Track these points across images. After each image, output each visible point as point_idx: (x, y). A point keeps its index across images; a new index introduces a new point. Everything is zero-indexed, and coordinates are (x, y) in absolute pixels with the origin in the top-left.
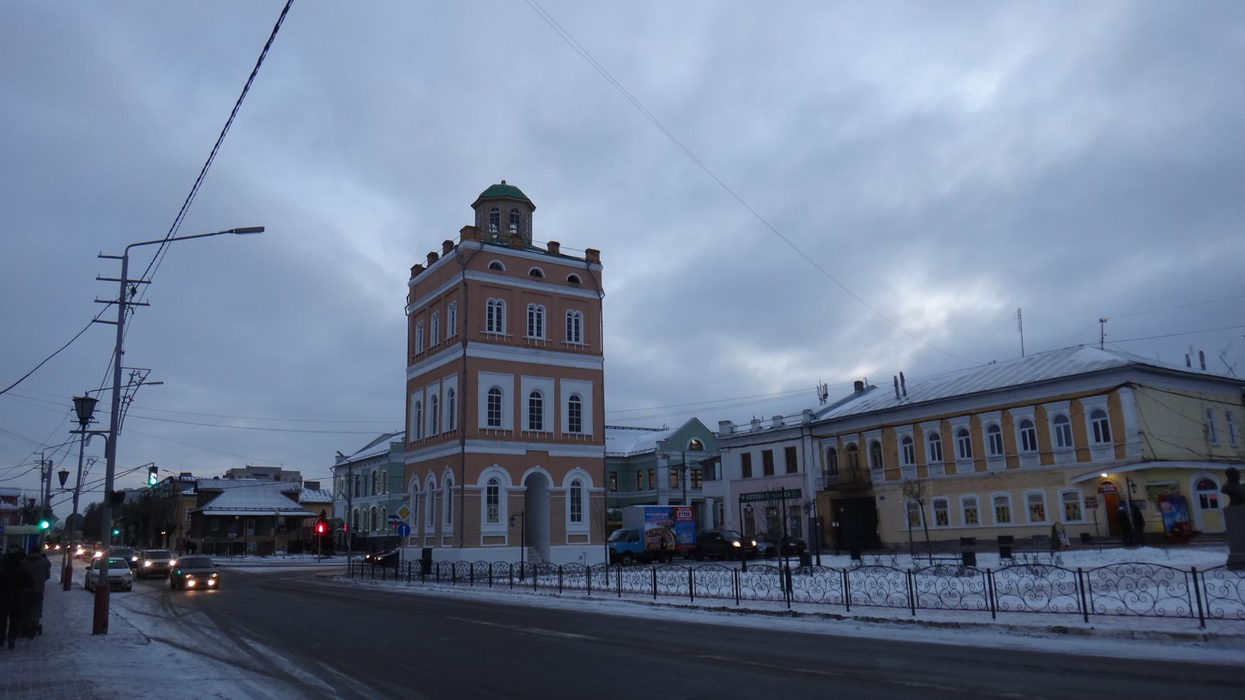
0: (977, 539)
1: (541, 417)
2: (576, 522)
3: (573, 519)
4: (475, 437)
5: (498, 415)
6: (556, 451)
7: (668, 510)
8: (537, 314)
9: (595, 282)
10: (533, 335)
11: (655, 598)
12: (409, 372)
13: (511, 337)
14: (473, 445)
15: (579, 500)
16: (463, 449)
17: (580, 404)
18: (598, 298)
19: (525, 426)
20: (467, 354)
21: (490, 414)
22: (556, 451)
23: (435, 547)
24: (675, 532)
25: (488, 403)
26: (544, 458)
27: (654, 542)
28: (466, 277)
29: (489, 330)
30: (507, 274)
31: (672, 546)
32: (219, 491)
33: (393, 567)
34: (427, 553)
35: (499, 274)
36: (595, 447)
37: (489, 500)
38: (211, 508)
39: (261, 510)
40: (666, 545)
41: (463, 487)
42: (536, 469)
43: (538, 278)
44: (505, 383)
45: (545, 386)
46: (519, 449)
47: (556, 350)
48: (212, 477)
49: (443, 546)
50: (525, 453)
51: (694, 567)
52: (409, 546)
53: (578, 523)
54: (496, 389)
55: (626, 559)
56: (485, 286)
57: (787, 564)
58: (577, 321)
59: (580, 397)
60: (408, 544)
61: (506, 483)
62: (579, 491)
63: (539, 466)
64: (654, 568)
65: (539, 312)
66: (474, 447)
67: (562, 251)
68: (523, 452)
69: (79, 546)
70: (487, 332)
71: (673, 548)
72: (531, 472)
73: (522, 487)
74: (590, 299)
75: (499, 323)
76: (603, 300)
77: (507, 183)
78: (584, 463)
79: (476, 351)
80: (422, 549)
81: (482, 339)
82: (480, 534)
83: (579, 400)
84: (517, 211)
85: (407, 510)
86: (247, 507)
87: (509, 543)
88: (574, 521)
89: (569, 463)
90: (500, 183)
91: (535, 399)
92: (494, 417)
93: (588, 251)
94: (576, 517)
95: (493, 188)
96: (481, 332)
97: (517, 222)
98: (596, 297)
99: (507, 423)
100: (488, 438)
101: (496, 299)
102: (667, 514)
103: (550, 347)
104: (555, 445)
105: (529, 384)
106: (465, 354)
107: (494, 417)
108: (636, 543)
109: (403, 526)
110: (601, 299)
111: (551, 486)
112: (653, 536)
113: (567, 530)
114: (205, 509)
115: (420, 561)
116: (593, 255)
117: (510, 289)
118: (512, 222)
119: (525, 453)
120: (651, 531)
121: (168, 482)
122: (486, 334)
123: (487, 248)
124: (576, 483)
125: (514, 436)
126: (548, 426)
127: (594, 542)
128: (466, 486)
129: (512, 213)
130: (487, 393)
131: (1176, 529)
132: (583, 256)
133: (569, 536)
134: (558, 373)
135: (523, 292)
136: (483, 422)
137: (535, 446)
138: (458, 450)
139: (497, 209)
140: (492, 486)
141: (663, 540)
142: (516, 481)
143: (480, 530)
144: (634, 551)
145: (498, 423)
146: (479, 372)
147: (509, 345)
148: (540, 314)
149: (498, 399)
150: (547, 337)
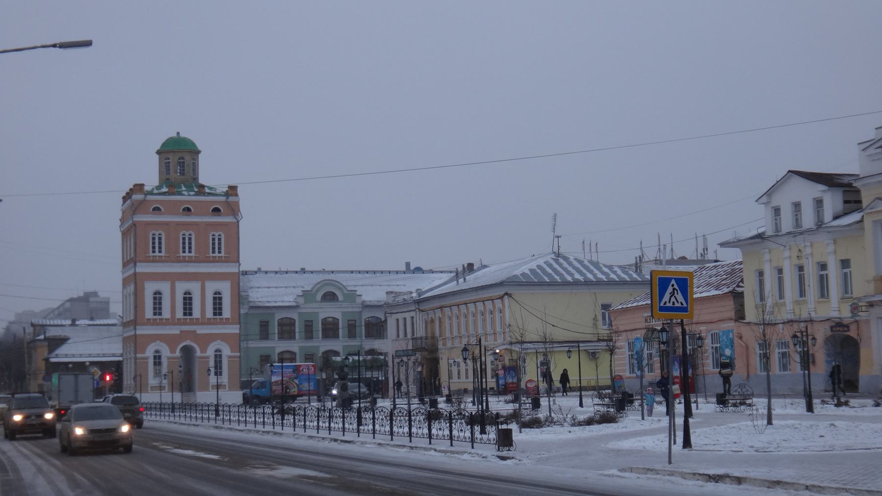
0: (468, 389)
4: (143, 324)
5: (160, 309)
6: (201, 330)
7: (292, 367)
9: (234, 210)
11: (196, 421)
12: (123, 273)
13: (168, 256)
15: (221, 362)
16: (135, 332)
19: (179, 314)
20: (137, 271)
22: (201, 330)
24: (298, 383)
26: (193, 335)
27: (277, 389)
28: (134, 219)
31: (295, 392)
32: (65, 338)
33: (291, 414)
36: (231, 326)
37: (155, 364)
38: (57, 355)
39: (104, 355)
43: (188, 213)
44: (164, 287)
45: (194, 287)
46: (175, 330)
56: (147, 224)
58: (220, 239)
59: (221, 292)
61: (166, 352)
63: (189, 341)
65: (190, 236)
66: (142, 331)
68: (178, 332)
69: (367, 392)
72: (188, 344)
73: (178, 354)
75: (160, 248)
76: (240, 222)
77: (182, 135)
78: (223, 337)
79: (142, 268)
81: (148, 260)
83: (221, 295)
84: (183, 158)
86: (90, 353)
89: (212, 338)
90: (175, 135)
92: (158, 310)
96: (147, 255)
98: (235, 220)
99: (166, 314)
100: (153, 324)
101: (157, 231)
102: (292, 370)
103: (197, 260)
105: (181, 287)
106: (135, 271)
107: (158, 310)
108: (264, 390)
110: (238, 222)
111: (198, 353)
112: (278, 385)
114: (51, 356)
116: (233, 190)
117: (167, 224)
121: (68, 305)
122: (180, 256)
123: (149, 197)
126: (196, 313)
127: (231, 389)
129: (180, 161)
134: (202, 278)
135: (177, 224)
136: (149, 313)
137: (186, 328)
138: (133, 333)
139: (169, 159)
140: (157, 354)
142: (173, 351)
143: (148, 383)
144: (261, 395)
145: (160, 314)
147: (167, 262)
149: (160, 298)
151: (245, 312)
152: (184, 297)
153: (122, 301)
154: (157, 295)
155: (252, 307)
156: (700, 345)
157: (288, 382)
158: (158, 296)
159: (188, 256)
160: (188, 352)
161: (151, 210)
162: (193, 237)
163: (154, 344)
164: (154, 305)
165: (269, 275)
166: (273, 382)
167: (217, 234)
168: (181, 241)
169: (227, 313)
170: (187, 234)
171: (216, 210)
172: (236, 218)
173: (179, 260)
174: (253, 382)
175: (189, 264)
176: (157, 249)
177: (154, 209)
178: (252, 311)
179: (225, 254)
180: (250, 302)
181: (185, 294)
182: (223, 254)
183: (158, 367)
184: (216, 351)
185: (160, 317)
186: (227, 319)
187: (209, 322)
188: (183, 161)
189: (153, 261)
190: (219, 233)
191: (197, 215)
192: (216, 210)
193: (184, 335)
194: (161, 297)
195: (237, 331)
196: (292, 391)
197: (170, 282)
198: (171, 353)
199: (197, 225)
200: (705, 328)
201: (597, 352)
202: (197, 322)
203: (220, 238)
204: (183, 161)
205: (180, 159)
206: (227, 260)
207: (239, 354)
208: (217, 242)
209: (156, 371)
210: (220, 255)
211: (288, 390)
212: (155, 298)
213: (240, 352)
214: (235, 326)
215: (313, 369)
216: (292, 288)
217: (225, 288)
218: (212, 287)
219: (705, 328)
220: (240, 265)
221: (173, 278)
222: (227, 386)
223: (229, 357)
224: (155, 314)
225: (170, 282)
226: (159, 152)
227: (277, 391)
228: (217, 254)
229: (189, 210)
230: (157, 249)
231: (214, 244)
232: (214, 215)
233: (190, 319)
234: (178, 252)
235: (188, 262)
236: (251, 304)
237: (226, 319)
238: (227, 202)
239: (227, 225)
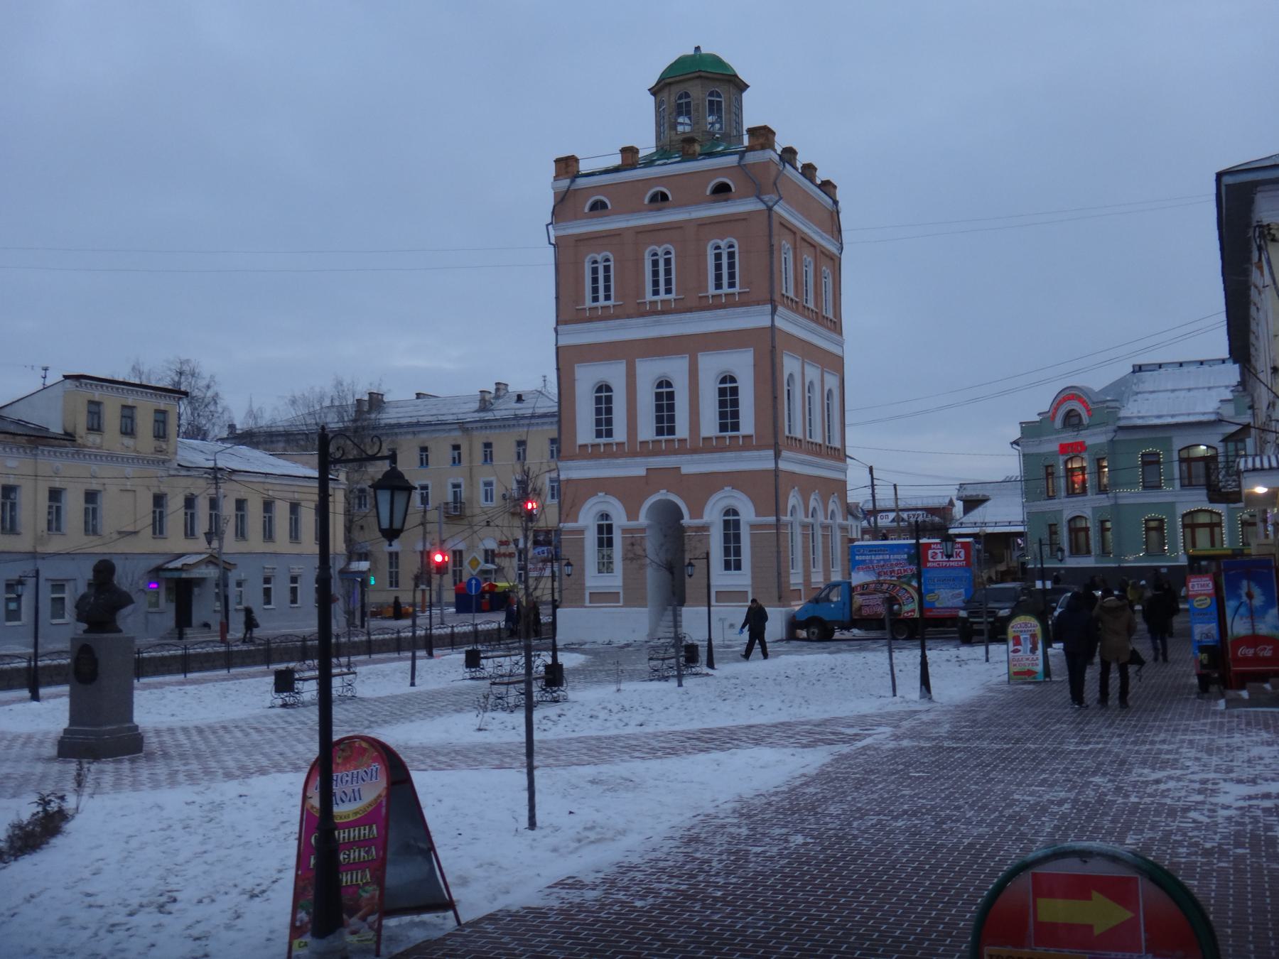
2: (733, 572)
3: (727, 566)
4: (572, 458)
6: (691, 466)
14: (569, 469)
15: (737, 538)
17: (672, 393)
22: (691, 466)
25: (654, 403)
26: (673, 478)
31: (913, 611)
36: (756, 453)
40: (900, 610)
41: (778, 520)
42: (662, 495)
43: (604, 212)
44: (614, 374)
45: (675, 368)
47: (690, 310)
49: (587, 604)
53: (737, 572)
54: (730, 376)
62: (737, 523)
63: (664, 491)
67: (584, 167)
68: (641, 472)
71: (916, 615)
72: (664, 498)
73: (643, 520)
74: (750, 213)
77: (704, 51)
82: (584, 589)
84: (687, 95)
88: (730, 569)
89: (712, 482)
90: (691, 52)
91: (665, 390)
92: (604, 424)
94: (732, 563)
95: (681, 62)
97: (688, 113)
98: (761, 206)
101: (599, 254)
102: (906, 556)
103: (682, 308)
104: (688, 457)
105: (649, 371)
107: (604, 424)
115: (1171, 635)
118: (680, 114)
120: (864, 586)
125: (635, 449)
133: (717, 592)
134: (691, 346)
135: (638, 233)
139: (719, 96)
140: (605, 522)
141: (891, 601)
143: (584, 584)
146: (637, 360)
147: (617, 317)
151: (1109, 439)
153: (846, 428)
154: (603, 394)
155: (1121, 428)
156: (949, 553)
157: (895, 586)
158: (604, 394)
160: (669, 518)
164: (658, 422)
165: (1185, 369)
166: (856, 587)
172: (762, 201)
173: (644, 312)
175: (664, 318)
176: (601, 294)
178: (1121, 436)
180: (1119, 419)
183: (605, 551)
184: (727, 513)
186: (682, 441)
188: (687, 100)
189: (590, 320)
191: (681, 205)
192: (722, 190)
193: (653, 479)
194: (611, 396)
196: (906, 608)
197: (624, 361)
198: (757, 516)
199: (619, 235)
200: (312, 866)
201: (165, 639)
202: (683, 448)
204: (687, 100)
205: (680, 98)
209: (603, 558)
211: (896, 607)
212: (598, 400)
214: (763, 453)
215: (962, 554)
216: (1206, 390)
217: (742, 364)
218: (712, 366)
219: (312, 866)
221: (628, 352)
223: (753, 526)
226: (655, 91)
227: (867, 609)
229: (664, 197)
230: (601, 294)
231: (718, 267)
232: (715, 201)
234: (640, 292)
235: (663, 313)
236: (1122, 423)
238: (741, 166)
239: (744, 219)
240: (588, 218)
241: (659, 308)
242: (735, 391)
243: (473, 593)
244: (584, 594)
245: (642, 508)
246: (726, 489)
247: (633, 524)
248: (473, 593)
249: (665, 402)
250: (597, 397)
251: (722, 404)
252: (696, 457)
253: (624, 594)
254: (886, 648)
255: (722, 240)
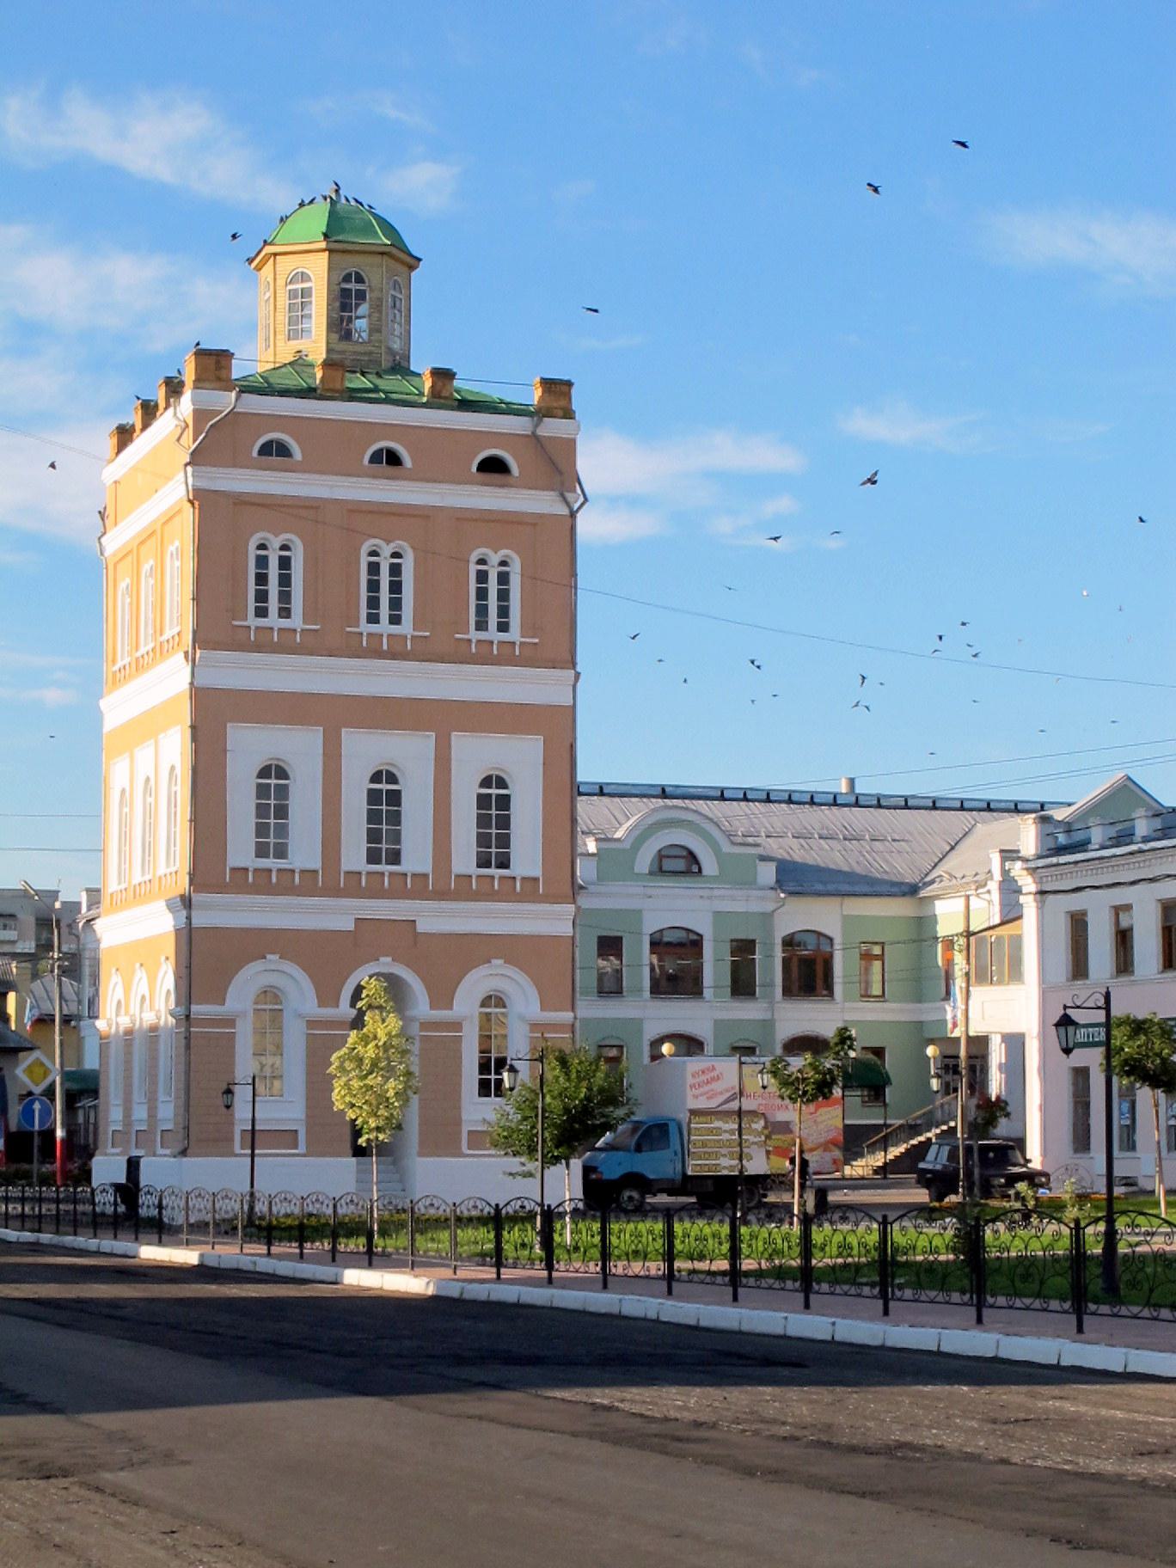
1: (398, 833)
4: (221, 888)
5: (504, 841)
8: (281, 558)
10: (378, 622)
18: (565, 511)
19: (354, 855)
21: (483, 840)
22: (435, 918)
23: (147, 1155)
29: (478, 629)
30: (414, 477)
34: (133, 1165)
35: (502, 486)
48: (1076, 1051)
50: (351, 927)
51: (829, 1216)
52: (160, 1151)
54: (277, 767)
55: (627, 1194)
57: (1111, 1236)
60: (106, 1147)
63: (389, 959)
64: (885, 1217)
70: (253, 621)
80: (126, 1158)
82: (233, 1124)
85: (42, 1064)
87: (309, 1144)
91: (494, 791)
93: (549, 385)
99: (305, 852)
100: (256, 889)
101: (388, 542)
103: (423, 653)
109: (32, 1102)
110: (573, 515)
113: (464, 1117)
117: (313, 507)
119: (351, 927)
122: (470, 641)
124: (270, 995)
126: (417, 856)
128: (194, 1008)
130: (255, 774)
131: (1127, 1068)
132: (535, 396)
133: (470, 1132)
142: (327, 996)
145: (281, 852)
146: (343, 730)
148: (399, 565)
149: (283, 792)
150: (306, 618)
152: (370, 792)
159: (389, 636)
161: (255, 453)
162: (515, 570)
163: (255, 967)
167: (494, 559)
168: (473, 585)
169: (527, 857)
170: (386, 550)
171: (494, 466)
174: (50, 1099)
176: (273, 604)
177: (266, 450)
179: (305, 622)
181: (376, 777)
182: (514, 634)
185: (282, 863)
186: (421, 877)
187: (462, 890)
188: (360, 287)
189: (258, 648)
190: (504, 552)
191: (422, 476)
192: (494, 466)
195: (566, 929)
198: (431, 1008)
199: (317, 508)
202: (419, 888)
203: (399, 565)
204: (360, 287)
206: (530, 658)
207: (571, 1015)
208: (493, 587)
210: (284, 623)
212: (262, 791)
213: (573, 1009)
220: (578, 675)
222: (302, 1137)
224: (261, 851)
225: (179, 727)
228: (492, 634)
229: (393, 459)
233: (502, 878)
237: (524, 879)
240: (368, 476)
241: (385, 647)
242: (395, 798)
243: (37, 1127)
244: (232, 1133)
245: (345, 987)
246: (495, 962)
247: (328, 1012)
248: (37, 1127)
249: (384, 807)
250: (259, 786)
251: (483, 821)
252: (444, 905)
253: (307, 1132)
254: (92, 1231)
255: (276, 536)
